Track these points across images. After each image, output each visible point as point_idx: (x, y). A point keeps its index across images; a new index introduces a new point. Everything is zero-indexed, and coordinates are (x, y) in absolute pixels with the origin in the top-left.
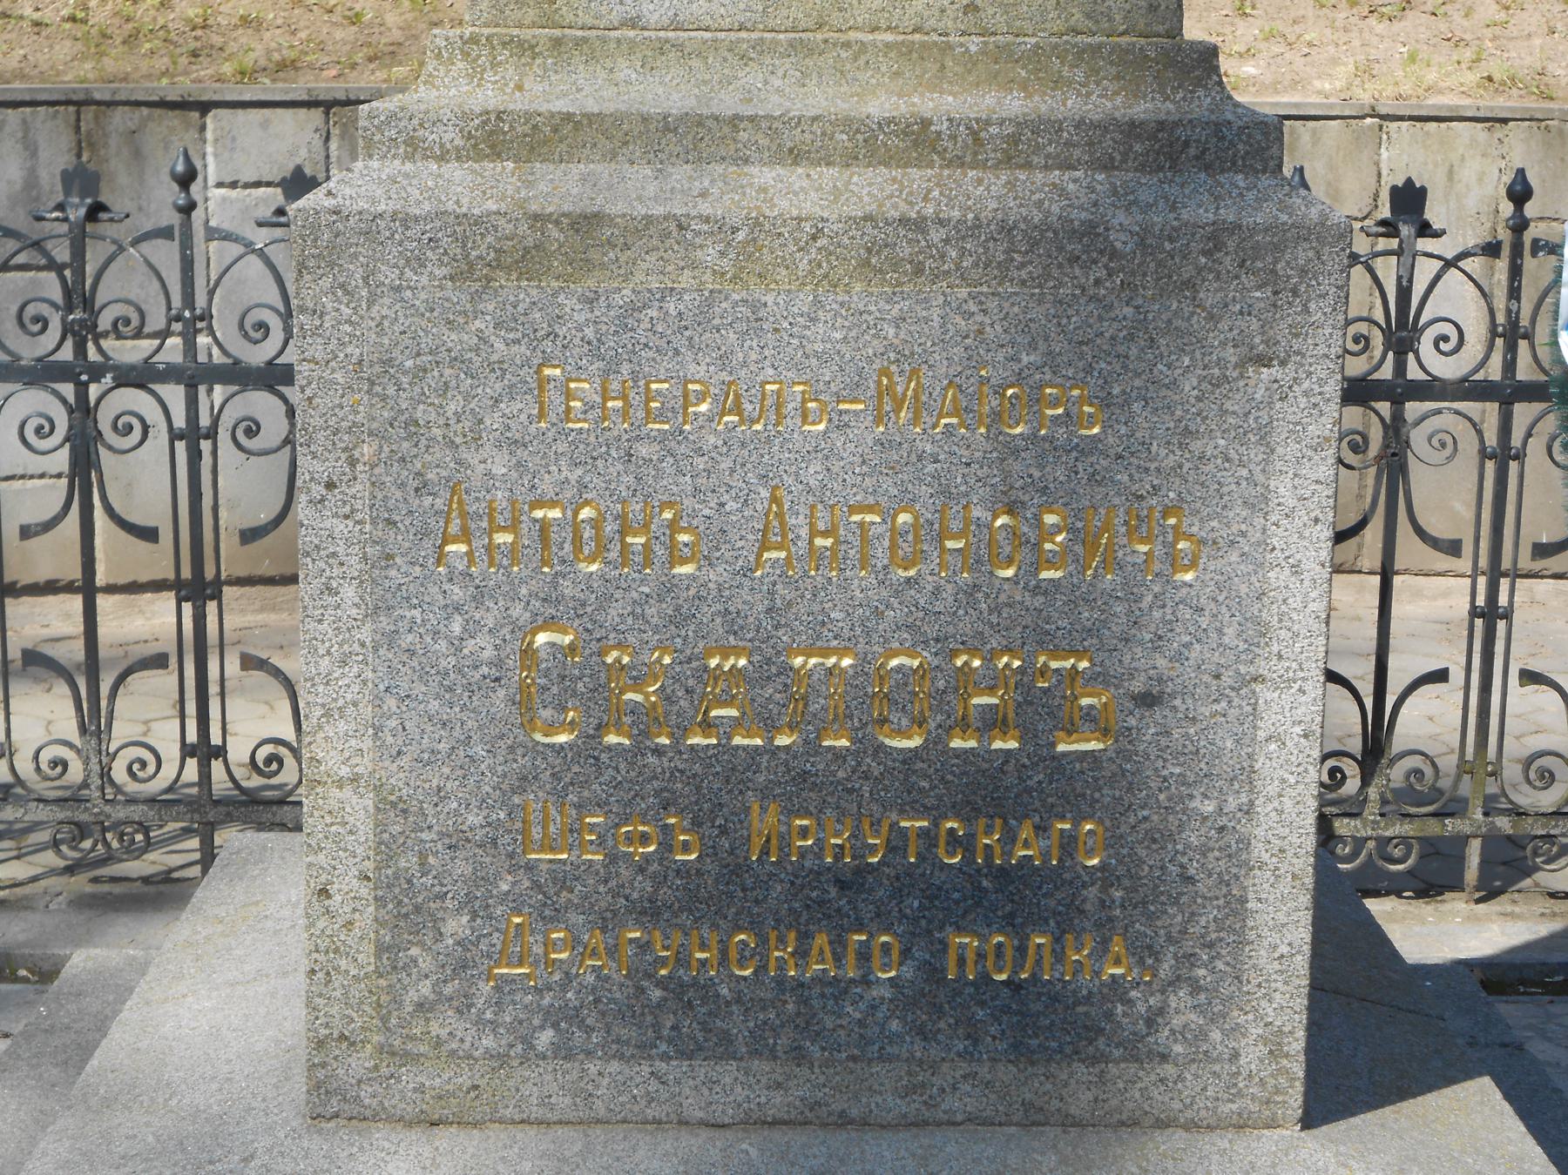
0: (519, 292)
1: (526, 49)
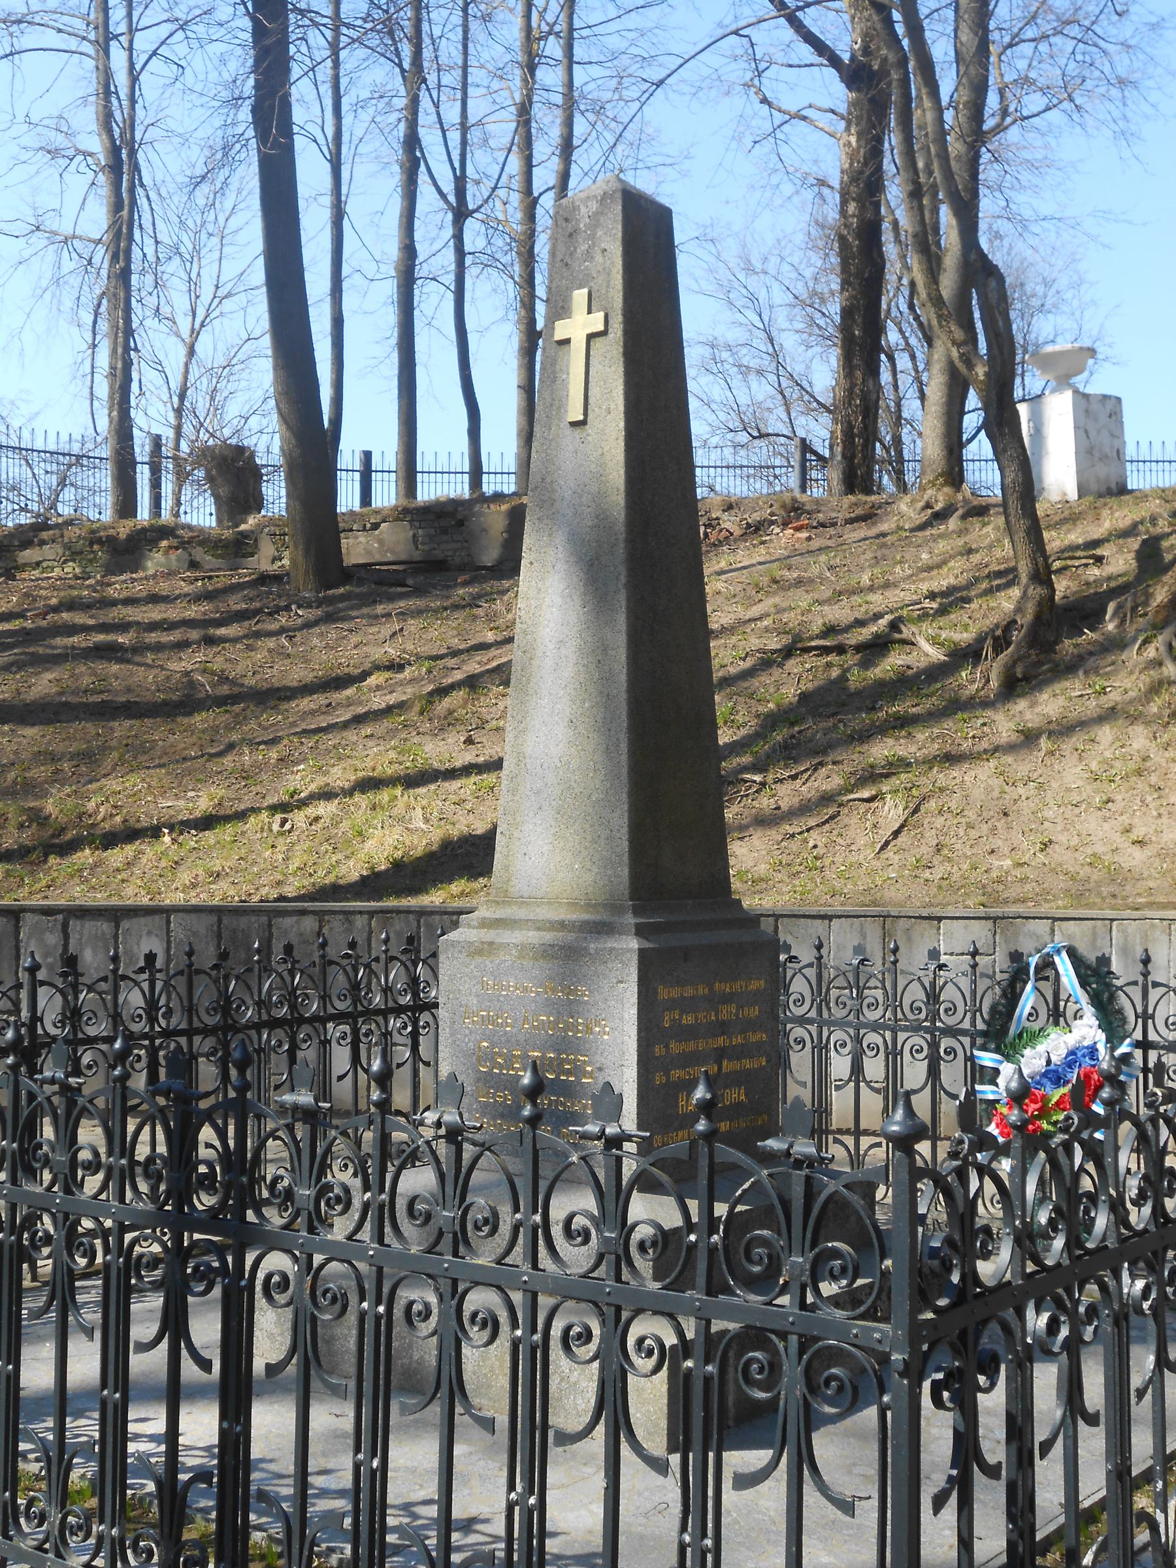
0: (478, 959)
1: (497, 903)
